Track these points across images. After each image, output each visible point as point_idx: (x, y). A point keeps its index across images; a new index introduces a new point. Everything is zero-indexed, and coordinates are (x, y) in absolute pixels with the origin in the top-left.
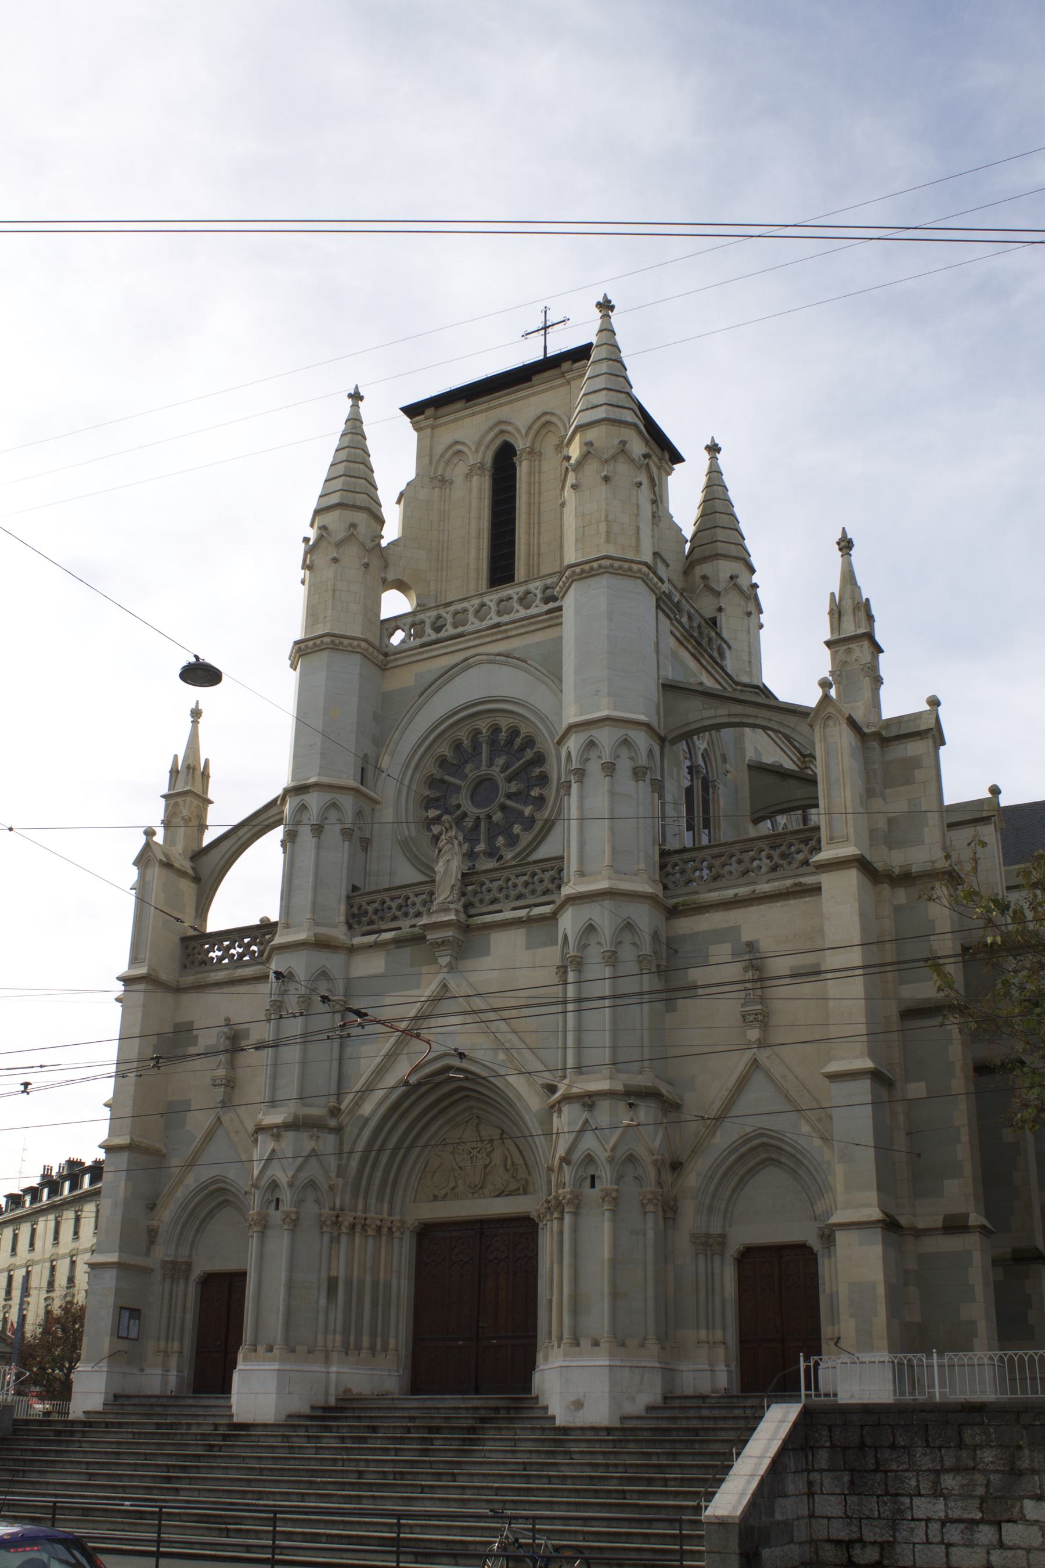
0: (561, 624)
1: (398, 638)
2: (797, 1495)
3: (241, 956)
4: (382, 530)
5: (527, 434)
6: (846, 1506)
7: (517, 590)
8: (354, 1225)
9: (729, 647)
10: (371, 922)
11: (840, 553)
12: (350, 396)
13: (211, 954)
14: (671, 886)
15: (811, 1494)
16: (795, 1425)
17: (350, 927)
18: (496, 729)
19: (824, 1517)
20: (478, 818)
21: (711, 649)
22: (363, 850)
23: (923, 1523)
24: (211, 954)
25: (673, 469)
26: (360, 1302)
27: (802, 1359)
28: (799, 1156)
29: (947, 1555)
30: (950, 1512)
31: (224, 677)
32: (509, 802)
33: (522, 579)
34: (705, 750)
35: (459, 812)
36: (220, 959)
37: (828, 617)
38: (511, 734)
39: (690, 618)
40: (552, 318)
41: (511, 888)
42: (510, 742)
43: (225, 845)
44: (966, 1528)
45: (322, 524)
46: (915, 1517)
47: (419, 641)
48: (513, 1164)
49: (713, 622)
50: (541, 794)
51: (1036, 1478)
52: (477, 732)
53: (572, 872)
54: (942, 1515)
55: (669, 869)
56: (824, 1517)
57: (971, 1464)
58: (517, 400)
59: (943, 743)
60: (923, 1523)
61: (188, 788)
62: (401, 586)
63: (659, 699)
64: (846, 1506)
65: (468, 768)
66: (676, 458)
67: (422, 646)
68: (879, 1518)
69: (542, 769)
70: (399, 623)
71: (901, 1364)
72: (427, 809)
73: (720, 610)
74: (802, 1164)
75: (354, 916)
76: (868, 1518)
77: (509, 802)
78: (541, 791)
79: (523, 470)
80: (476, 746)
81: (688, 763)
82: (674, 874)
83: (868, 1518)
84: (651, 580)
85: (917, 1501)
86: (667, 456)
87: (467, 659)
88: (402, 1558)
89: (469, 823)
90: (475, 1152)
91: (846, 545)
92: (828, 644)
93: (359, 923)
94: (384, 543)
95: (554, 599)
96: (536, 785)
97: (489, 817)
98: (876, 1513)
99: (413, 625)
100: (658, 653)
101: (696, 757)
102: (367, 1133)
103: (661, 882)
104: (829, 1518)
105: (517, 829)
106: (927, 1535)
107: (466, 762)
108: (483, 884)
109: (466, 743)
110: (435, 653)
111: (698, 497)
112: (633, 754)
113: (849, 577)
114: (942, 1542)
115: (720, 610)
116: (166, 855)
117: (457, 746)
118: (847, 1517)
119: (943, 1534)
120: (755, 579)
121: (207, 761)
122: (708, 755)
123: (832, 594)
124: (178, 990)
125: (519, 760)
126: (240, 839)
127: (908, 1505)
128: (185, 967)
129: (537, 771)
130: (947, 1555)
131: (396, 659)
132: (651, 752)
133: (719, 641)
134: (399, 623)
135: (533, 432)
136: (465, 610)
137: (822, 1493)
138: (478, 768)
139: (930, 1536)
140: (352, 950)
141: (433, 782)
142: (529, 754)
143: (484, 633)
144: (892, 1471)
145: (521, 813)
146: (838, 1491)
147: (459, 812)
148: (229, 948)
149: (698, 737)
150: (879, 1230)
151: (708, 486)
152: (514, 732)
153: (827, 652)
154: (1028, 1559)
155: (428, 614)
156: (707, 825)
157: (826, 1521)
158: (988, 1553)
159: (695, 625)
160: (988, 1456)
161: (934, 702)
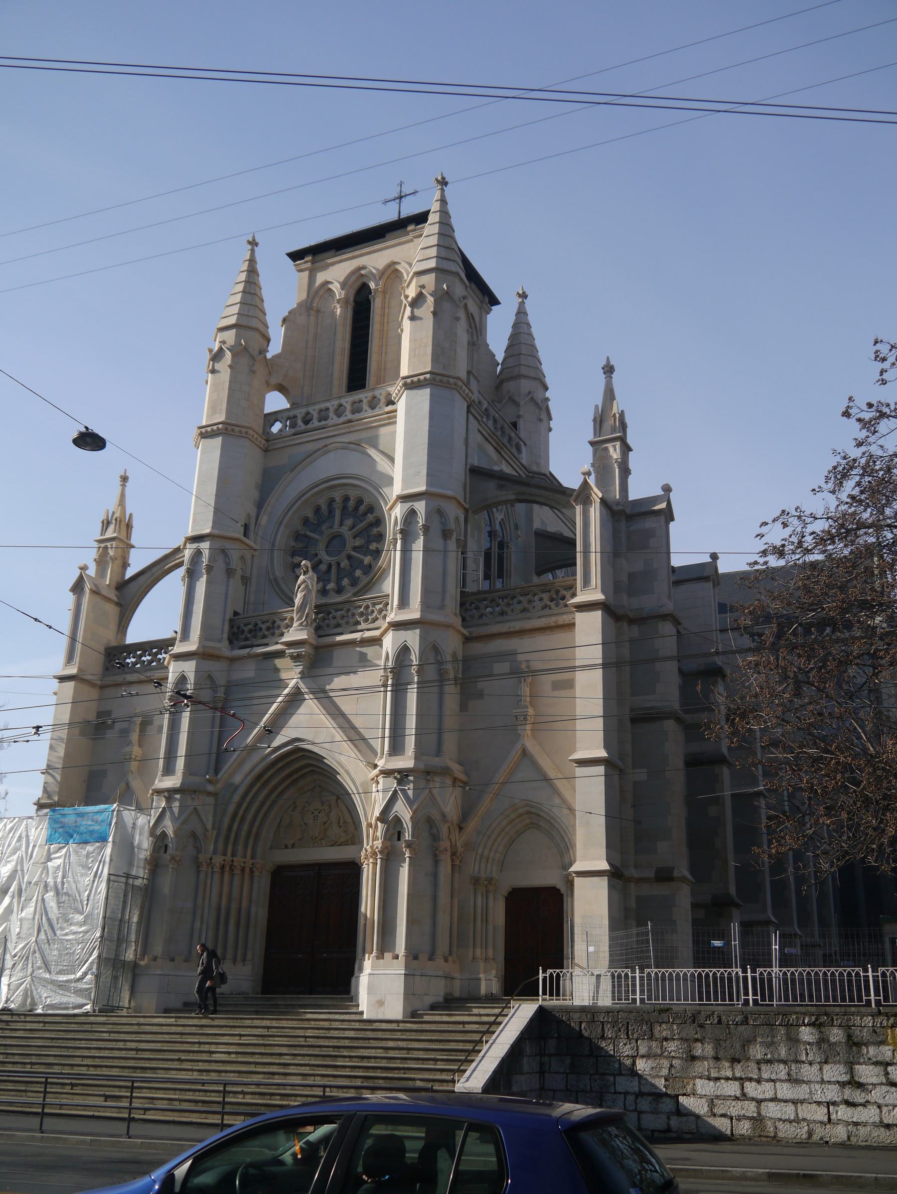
0: (395, 422)
1: (276, 428)
2: (531, 1073)
3: (151, 662)
4: (268, 346)
5: (380, 279)
6: (567, 1082)
7: (366, 395)
8: (223, 865)
9: (525, 444)
10: (246, 639)
11: (605, 376)
12: (249, 243)
13: (128, 661)
14: (468, 618)
15: (542, 1073)
16: (532, 1020)
17: (231, 642)
18: (346, 499)
19: (551, 1090)
20: (330, 564)
21: (511, 445)
22: (243, 585)
23: (622, 1096)
24: (128, 661)
25: (491, 310)
26: (227, 924)
27: (541, 971)
28: (552, 821)
29: (639, 1119)
30: (642, 1087)
31: (108, 444)
32: (353, 553)
33: (371, 387)
34: (502, 519)
35: (316, 559)
36: (135, 664)
37: (592, 424)
38: (357, 503)
39: (495, 421)
40: (406, 190)
41: (350, 616)
42: (356, 508)
43: (142, 578)
44: (654, 1100)
45: (222, 340)
46: (617, 1090)
47: (293, 431)
48: (345, 822)
49: (515, 425)
50: (377, 548)
51: (706, 1063)
52: (332, 501)
53: (395, 606)
54: (636, 1089)
55: (467, 606)
56: (551, 1090)
57: (659, 1051)
58: (374, 252)
59: (672, 519)
60: (622, 1096)
61: (115, 535)
62: (282, 389)
63: (465, 480)
64: (567, 1082)
65: (324, 527)
66: (494, 301)
67: (294, 435)
68: (591, 1091)
69: (379, 529)
70: (279, 416)
71: (619, 976)
72: (293, 556)
73: (519, 417)
74: (554, 826)
75: (234, 634)
76: (583, 1091)
77: (353, 553)
78: (377, 546)
79: (377, 305)
80: (331, 511)
81: (489, 529)
82: (471, 610)
83: (583, 1091)
84: (464, 391)
85: (619, 1079)
86: (487, 299)
87: (326, 446)
88: (226, 1117)
89: (323, 567)
90: (316, 813)
91: (609, 370)
92: (592, 443)
93: (237, 639)
94: (269, 356)
95: (393, 403)
96: (373, 541)
97: (338, 564)
98: (589, 1087)
99: (289, 418)
100: (467, 446)
101: (495, 525)
102: (236, 798)
103: (461, 616)
104: (554, 1091)
105: (358, 573)
106: (625, 1104)
107: (323, 522)
108: (330, 613)
109: (324, 508)
110: (304, 440)
111: (508, 331)
112: (443, 520)
113: (609, 395)
114: (635, 1110)
115: (519, 417)
116: (96, 585)
117: (318, 510)
118: (568, 1090)
119: (636, 1104)
120: (548, 394)
121: (131, 515)
122: (504, 523)
123: (597, 406)
124: (102, 687)
125: (362, 522)
126: (153, 574)
127: (613, 1082)
128: (107, 669)
129: (375, 531)
130: (639, 1119)
131: (358, 425)
132: (457, 519)
133: (517, 439)
134: (279, 416)
135: (385, 277)
136: (327, 409)
137: (550, 1072)
138: (331, 527)
139: (627, 1105)
140: (232, 660)
141: (297, 536)
142: (370, 517)
143: (341, 426)
144: (602, 1056)
145: (362, 561)
146: (561, 1070)
147: (316, 559)
148: (141, 656)
149: (497, 510)
150: (606, 878)
151: (516, 326)
152: (360, 501)
153: (590, 449)
154: (697, 1123)
155: (300, 411)
156: (500, 575)
157: (552, 1093)
158: (668, 1118)
159: (499, 426)
160: (672, 1046)
161: (667, 489)
